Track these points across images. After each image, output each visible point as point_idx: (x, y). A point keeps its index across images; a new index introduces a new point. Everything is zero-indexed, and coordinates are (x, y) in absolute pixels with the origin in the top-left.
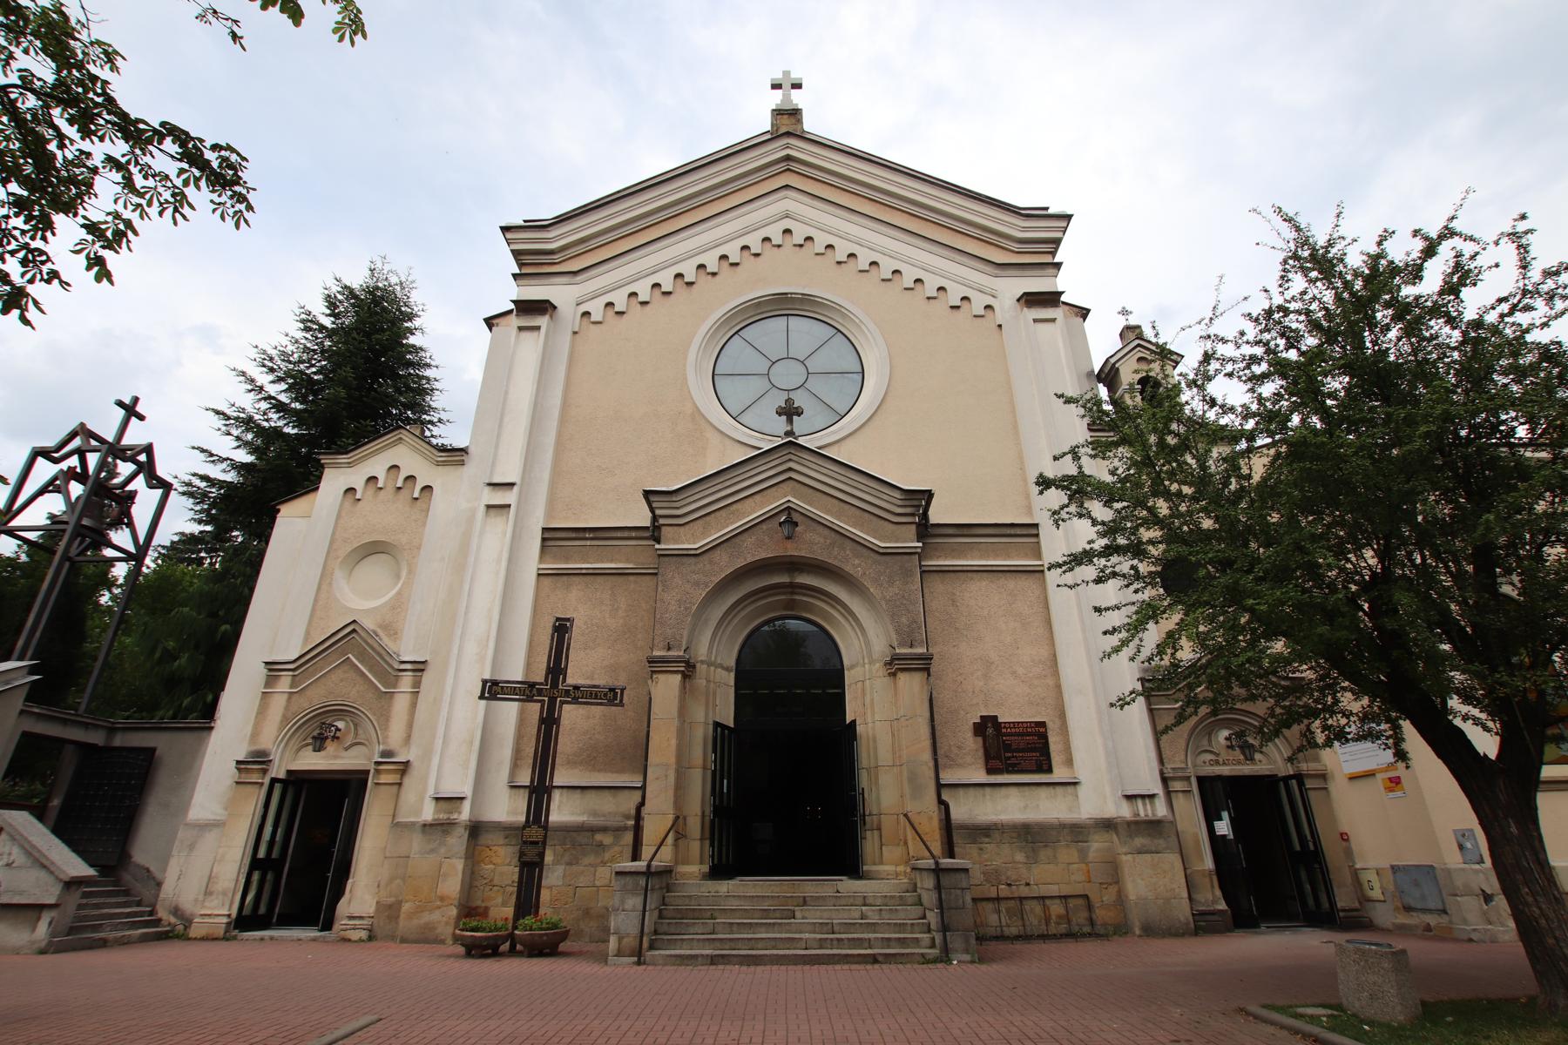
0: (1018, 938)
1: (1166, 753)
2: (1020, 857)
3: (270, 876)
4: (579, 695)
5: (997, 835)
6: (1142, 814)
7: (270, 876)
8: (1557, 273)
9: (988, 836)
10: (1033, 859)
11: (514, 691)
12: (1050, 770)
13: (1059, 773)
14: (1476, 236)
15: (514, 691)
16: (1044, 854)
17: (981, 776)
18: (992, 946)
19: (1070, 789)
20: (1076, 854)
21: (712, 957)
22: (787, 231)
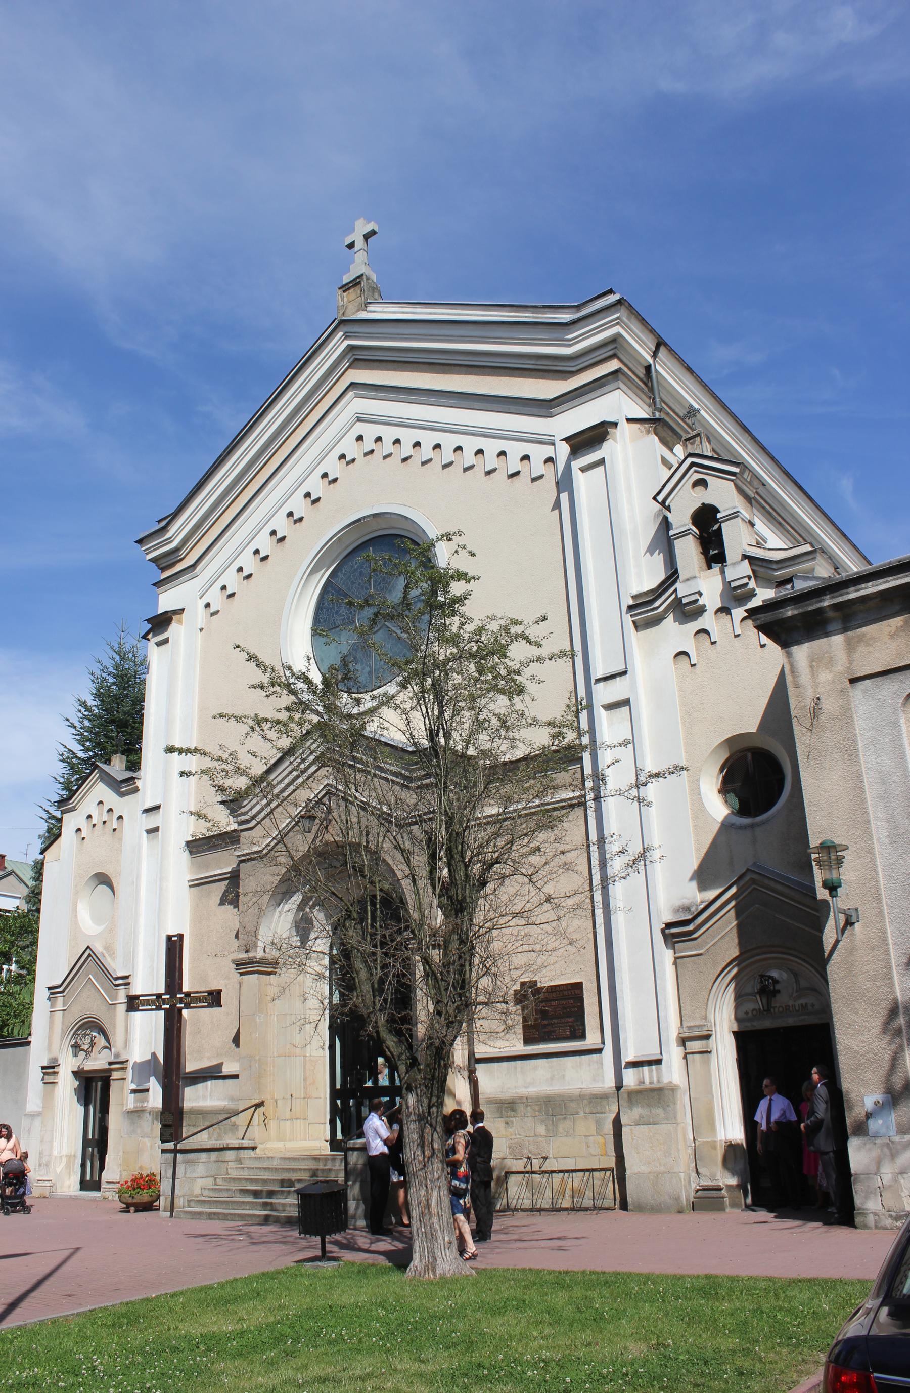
0: (531, 1210)
1: (687, 1009)
2: (541, 1130)
3: (88, 1178)
4: (191, 1000)
5: (521, 1108)
6: (647, 1081)
7: (88, 1178)
8: (666, 524)
9: (513, 1110)
10: (552, 1133)
11: (147, 1003)
12: (583, 1036)
13: (592, 1039)
14: (208, 751)
15: (147, 1003)
16: (563, 1126)
17: (520, 1048)
18: (44, 1161)
19: (595, 1057)
20: (593, 1126)
21: (211, 1213)
22: (360, 438)
